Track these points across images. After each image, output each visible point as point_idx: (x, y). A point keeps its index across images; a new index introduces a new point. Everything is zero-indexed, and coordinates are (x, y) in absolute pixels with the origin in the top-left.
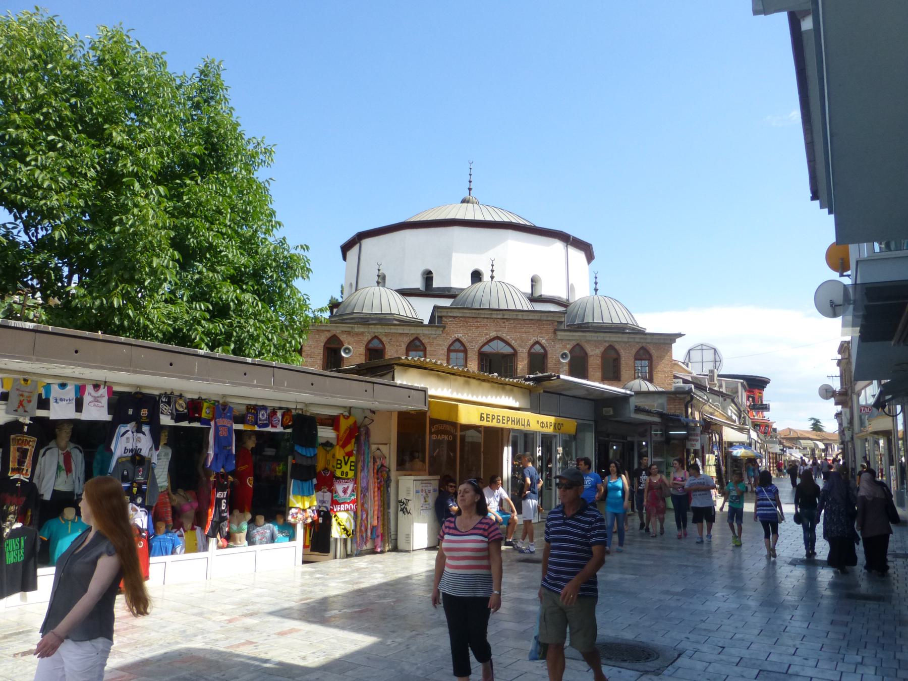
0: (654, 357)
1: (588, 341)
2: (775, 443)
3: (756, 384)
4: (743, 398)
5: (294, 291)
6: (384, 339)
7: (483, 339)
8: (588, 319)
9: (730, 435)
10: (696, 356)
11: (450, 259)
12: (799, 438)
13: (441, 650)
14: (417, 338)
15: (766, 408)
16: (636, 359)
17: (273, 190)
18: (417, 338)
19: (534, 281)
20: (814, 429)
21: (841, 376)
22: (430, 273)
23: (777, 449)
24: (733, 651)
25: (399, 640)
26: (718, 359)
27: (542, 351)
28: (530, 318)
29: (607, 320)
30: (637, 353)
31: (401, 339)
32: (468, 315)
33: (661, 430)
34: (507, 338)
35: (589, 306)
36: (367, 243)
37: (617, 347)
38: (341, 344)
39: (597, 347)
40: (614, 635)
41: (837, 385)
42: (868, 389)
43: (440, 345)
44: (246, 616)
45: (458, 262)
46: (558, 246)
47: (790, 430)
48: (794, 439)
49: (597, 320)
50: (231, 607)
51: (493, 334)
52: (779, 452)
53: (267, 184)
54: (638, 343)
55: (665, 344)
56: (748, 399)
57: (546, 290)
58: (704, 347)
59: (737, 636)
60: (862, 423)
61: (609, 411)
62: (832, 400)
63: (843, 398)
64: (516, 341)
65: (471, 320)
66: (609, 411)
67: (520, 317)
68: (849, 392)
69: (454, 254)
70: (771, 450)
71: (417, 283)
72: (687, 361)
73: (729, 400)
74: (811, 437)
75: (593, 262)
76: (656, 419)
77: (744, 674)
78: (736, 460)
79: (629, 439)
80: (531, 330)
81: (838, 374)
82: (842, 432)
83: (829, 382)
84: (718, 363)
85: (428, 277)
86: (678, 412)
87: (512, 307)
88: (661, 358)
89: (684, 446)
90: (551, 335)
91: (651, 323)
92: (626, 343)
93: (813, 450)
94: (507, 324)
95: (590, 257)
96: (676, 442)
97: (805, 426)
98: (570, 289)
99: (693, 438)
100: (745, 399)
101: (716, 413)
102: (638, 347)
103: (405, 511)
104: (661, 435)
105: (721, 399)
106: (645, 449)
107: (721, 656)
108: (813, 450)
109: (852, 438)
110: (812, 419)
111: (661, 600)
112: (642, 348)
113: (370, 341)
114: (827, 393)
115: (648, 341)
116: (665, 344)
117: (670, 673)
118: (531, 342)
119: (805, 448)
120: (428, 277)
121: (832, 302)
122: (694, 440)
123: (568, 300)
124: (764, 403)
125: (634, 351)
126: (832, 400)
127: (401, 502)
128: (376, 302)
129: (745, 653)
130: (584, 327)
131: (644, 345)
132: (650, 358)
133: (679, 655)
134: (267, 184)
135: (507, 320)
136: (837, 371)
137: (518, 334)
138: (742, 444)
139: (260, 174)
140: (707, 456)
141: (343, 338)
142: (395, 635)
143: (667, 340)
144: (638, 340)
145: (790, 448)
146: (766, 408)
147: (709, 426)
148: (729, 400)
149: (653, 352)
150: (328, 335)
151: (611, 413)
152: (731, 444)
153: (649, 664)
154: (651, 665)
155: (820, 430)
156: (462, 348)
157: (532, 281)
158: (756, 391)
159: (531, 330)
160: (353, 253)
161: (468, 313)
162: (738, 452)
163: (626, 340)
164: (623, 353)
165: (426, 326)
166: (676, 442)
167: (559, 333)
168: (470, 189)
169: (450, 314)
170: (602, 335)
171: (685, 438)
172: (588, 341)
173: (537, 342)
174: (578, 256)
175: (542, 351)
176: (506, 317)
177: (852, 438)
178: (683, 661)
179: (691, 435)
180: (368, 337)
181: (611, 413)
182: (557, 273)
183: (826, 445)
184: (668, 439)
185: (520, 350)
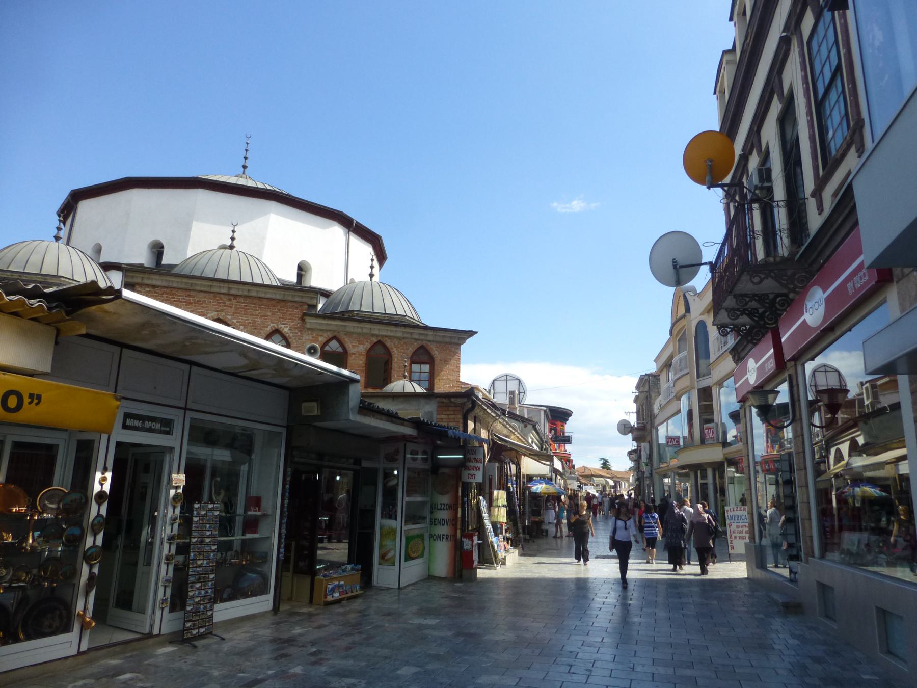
0: (437, 361)
1: (350, 334)
2: (574, 479)
3: (559, 416)
4: (544, 426)
8: (354, 307)
9: (529, 466)
10: (500, 386)
11: (188, 230)
12: (593, 476)
15: (568, 440)
16: (412, 362)
19: (302, 270)
20: (603, 468)
21: (638, 413)
23: (574, 485)
26: (522, 391)
28: (268, 296)
29: (378, 309)
30: (414, 354)
32: (175, 285)
33: (424, 452)
35: (357, 292)
36: (85, 207)
37: (388, 343)
41: (633, 420)
42: (670, 421)
45: (203, 233)
46: (337, 231)
47: (585, 468)
48: (589, 477)
49: (366, 308)
52: (576, 488)
54: (416, 340)
55: (451, 343)
56: (550, 432)
58: (509, 378)
60: (661, 459)
61: (311, 408)
62: (630, 436)
63: (641, 433)
65: (180, 293)
66: (311, 408)
67: (254, 294)
68: (648, 426)
69: (194, 223)
70: (569, 487)
71: (141, 257)
73: (530, 427)
74: (603, 474)
75: (387, 264)
76: (408, 431)
78: (535, 496)
79: (365, 464)
80: (269, 314)
81: (635, 410)
82: (637, 468)
83: (626, 418)
87: (247, 279)
88: (446, 361)
89: (459, 477)
90: (297, 322)
91: (434, 315)
92: (399, 339)
93: (604, 487)
94: (234, 302)
95: (381, 256)
96: (446, 470)
97: (596, 465)
99: (472, 464)
100: (547, 430)
101: (513, 437)
102: (416, 345)
104: (425, 460)
105: (521, 425)
106: (394, 482)
108: (604, 487)
109: (651, 474)
110: (602, 459)
112: (422, 347)
114: (625, 428)
115: (430, 338)
116: (451, 343)
119: (598, 485)
120: (158, 250)
121: (674, 261)
122: (473, 468)
124: (566, 434)
125: (411, 350)
126: (630, 436)
128: (35, 259)
130: (348, 316)
131: (424, 343)
132: (431, 361)
135: (236, 296)
136: (633, 407)
137: (250, 319)
138: (543, 478)
140: (495, 492)
143: (455, 339)
144: (416, 337)
145: (586, 484)
146: (568, 440)
147: (502, 452)
148: (530, 427)
149: (435, 353)
151: (316, 412)
152: (530, 478)
155: (608, 469)
158: (559, 423)
159: (269, 314)
161: (175, 282)
162: (539, 488)
163: (399, 335)
164: (395, 352)
166: (446, 470)
167: (308, 320)
168: (245, 167)
169: (146, 282)
170: (368, 326)
171: (461, 466)
172: (350, 334)
174: (363, 251)
176: (233, 292)
177: (651, 474)
179: (470, 460)
181: (316, 412)
182: (332, 261)
183: (615, 482)
184: (436, 467)
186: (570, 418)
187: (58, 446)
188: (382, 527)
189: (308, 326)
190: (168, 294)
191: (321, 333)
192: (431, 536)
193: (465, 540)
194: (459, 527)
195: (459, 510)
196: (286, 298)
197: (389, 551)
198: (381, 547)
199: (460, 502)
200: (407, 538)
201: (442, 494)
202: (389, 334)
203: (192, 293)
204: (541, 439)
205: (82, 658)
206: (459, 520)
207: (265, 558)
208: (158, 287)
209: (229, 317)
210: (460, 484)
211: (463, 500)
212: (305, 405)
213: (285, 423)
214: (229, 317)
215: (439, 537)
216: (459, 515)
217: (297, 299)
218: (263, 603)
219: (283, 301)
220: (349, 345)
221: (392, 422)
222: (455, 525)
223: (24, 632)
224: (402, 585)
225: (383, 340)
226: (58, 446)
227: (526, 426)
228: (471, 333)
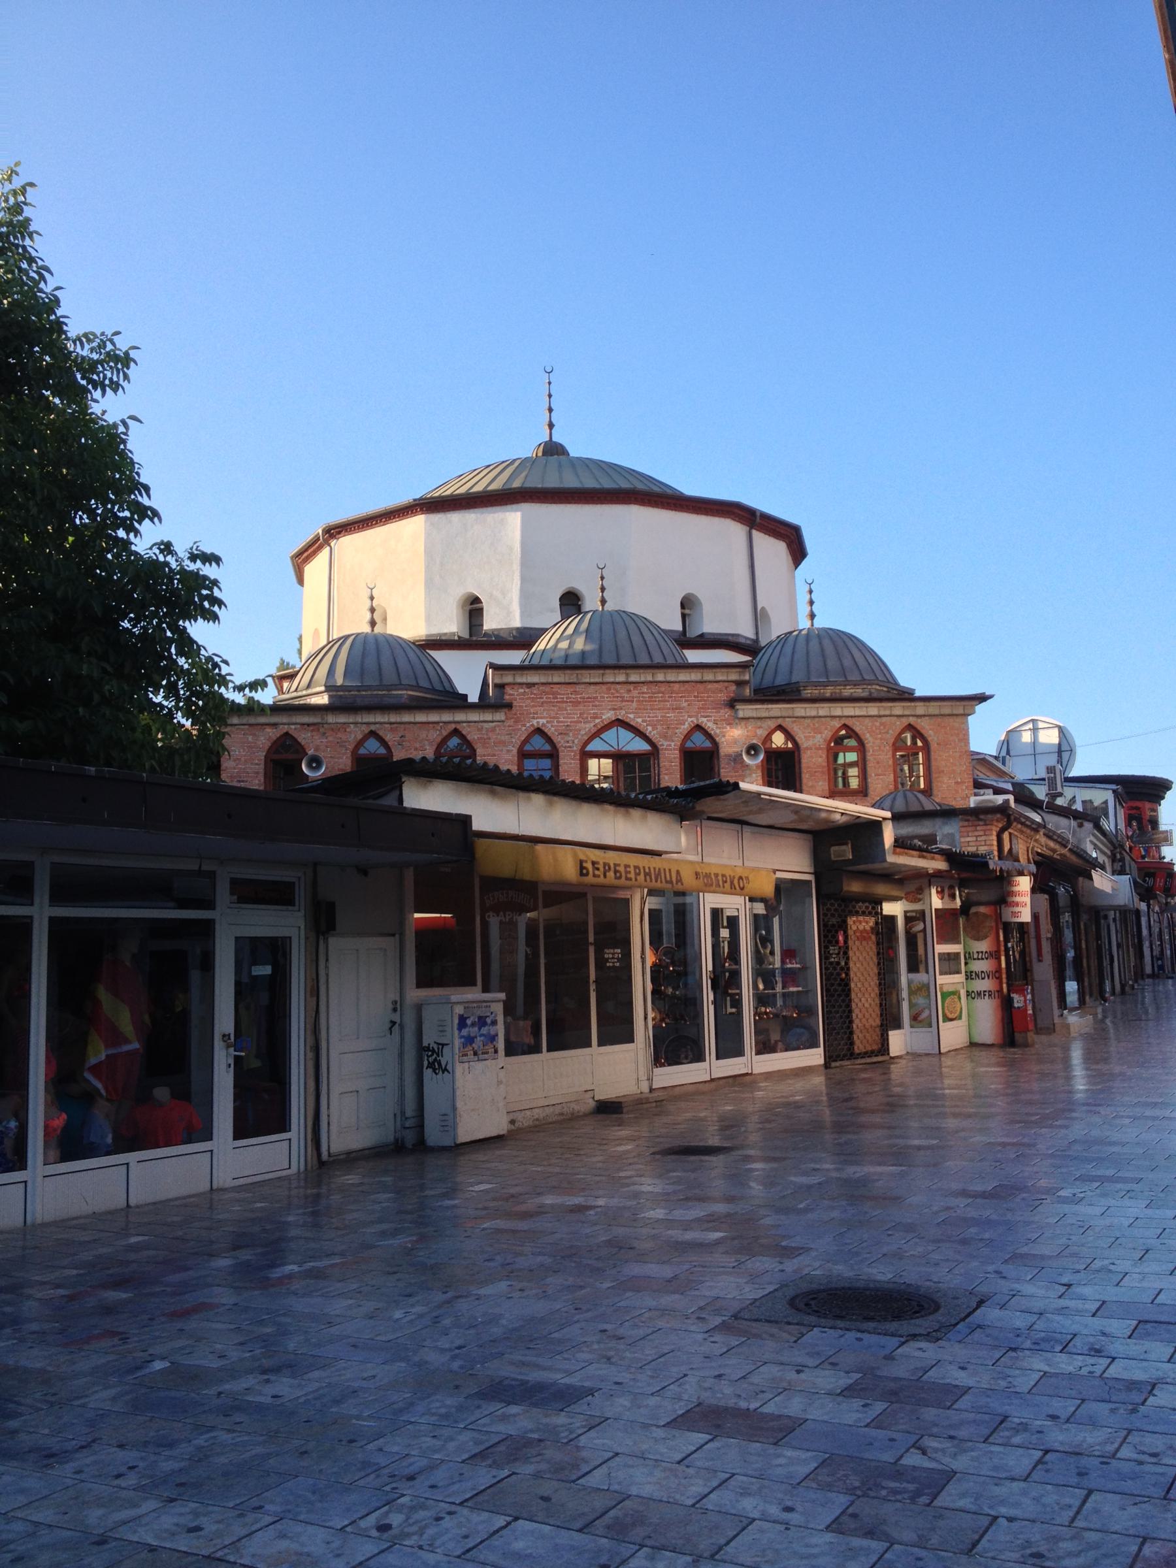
0: (934, 746)
3: (1141, 793)
5: (188, 646)
6: (388, 737)
7: (588, 727)
13: (504, 1322)
14: (456, 732)
17: (138, 445)
18: (456, 732)
19: (688, 604)
22: (476, 600)
24: (1087, 1291)
25: (418, 1309)
27: (708, 744)
31: (423, 734)
34: (638, 721)
36: (346, 544)
38: (300, 750)
39: (817, 731)
40: (851, 1274)
43: (503, 743)
44: (104, 1286)
50: (75, 1272)
51: (609, 716)
53: (121, 429)
57: (710, 624)
59: (1098, 1264)
64: (654, 727)
66: (846, 851)
72: (1004, 753)
73: (1088, 826)
77: (1107, 1330)
84: (1065, 756)
85: (474, 608)
86: (983, 850)
94: (635, 693)
98: (759, 616)
103: (438, 1067)
105: (1073, 823)
107: (1063, 1302)
111: (948, 1208)
113: (360, 743)
117: (960, 1337)
118: (686, 727)
120: (474, 608)
122: (1017, 904)
123: (757, 641)
127: (428, 1049)
129: (1111, 1293)
131: (912, 720)
133: (980, 1303)
134: (121, 429)
137: (659, 714)
139: (107, 407)
141: (304, 737)
142: (412, 1300)
150: (273, 734)
153: (918, 1321)
154: (923, 1324)
156: (547, 747)
157: (683, 606)
160: (316, 568)
165: (473, 706)
169: (519, 680)
173: (698, 727)
174: (771, 550)
175: (708, 744)
178: (990, 1314)
180: (356, 734)
185: (663, 744)
186: (1168, 794)
187: (214, 920)
188: (910, 983)
189: (741, 714)
190: (547, 693)
191: (759, 723)
192: (968, 994)
193: (1015, 996)
194: (1004, 980)
195: (1003, 958)
196: (706, 678)
197: (922, 1011)
198: (911, 1005)
199: (1003, 948)
200: (943, 994)
201: (978, 939)
202: (858, 712)
203: (579, 688)
204: (1111, 842)
205: (713, 1085)
206: (1004, 971)
207: (812, 1011)
208: (534, 684)
209: (632, 716)
210: (1001, 926)
211: (1006, 946)
212: (833, 849)
213: (812, 871)
214: (632, 716)
215: (979, 994)
216: (1003, 965)
217: (720, 678)
218: (815, 1057)
219: (701, 682)
220: (800, 737)
221: (924, 857)
222: (999, 978)
223: (666, 1059)
224: (943, 1051)
225: (849, 722)
226: (214, 920)
227: (1080, 825)
228: (982, 698)
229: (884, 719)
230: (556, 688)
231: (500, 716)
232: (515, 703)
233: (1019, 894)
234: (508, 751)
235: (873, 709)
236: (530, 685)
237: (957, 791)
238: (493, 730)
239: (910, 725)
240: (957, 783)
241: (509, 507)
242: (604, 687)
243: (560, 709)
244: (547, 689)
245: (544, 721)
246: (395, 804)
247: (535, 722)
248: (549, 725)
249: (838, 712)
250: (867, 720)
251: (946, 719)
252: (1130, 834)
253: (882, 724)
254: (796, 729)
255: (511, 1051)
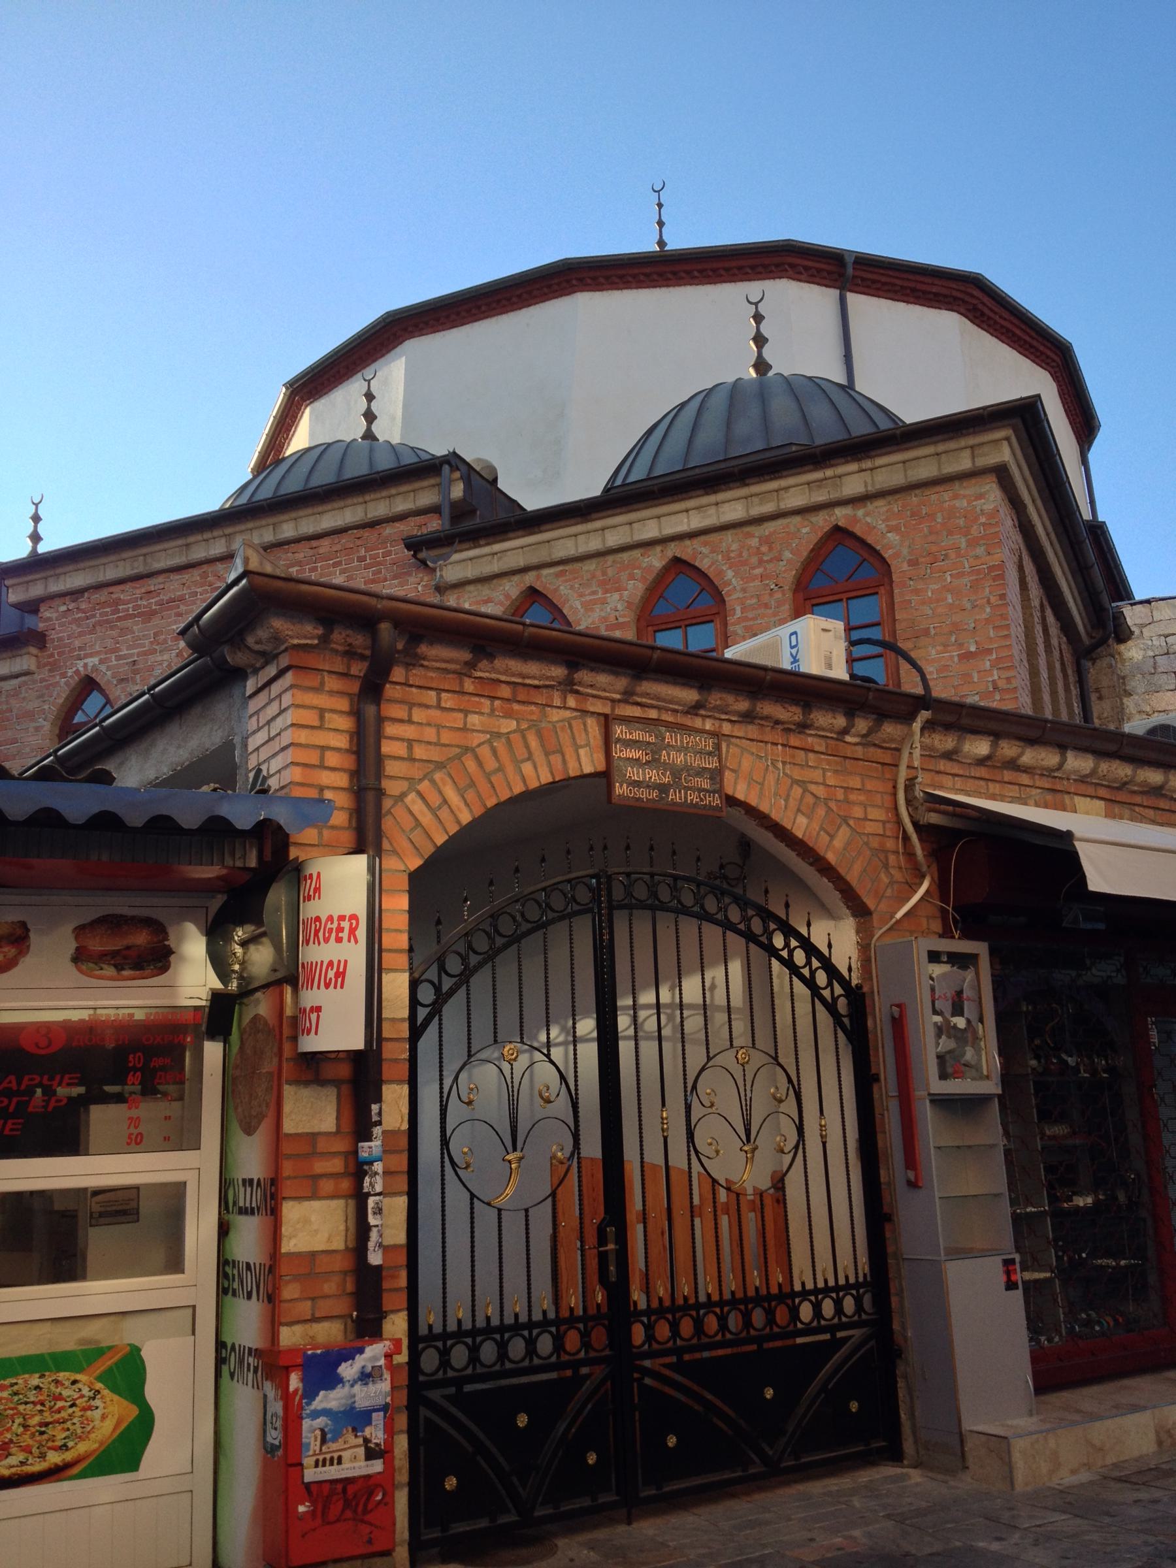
43: (30, 715)
131: (841, 515)
203: (152, 584)
229: (770, 527)
230: (118, 592)
231: (25, 661)
232: (53, 635)
233: (320, 930)
234: (37, 729)
235: (731, 506)
236: (76, 594)
237: (967, 676)
238: (16, 693)
239: (837, 529)
240: (967, 656)
241: (388, 356)
242: (196, 574)
243: (124, 631)
244: (102, 596)
245: (96, 660)
246: (741, 892)
247: (80, 665)
248: (103, 668)
249: (650, 531)
250: (729, 537)
251: (934, 496)
252: (732, 555)
253: (766, 540)
254: (564, 590)
255: (1017, 1219)
